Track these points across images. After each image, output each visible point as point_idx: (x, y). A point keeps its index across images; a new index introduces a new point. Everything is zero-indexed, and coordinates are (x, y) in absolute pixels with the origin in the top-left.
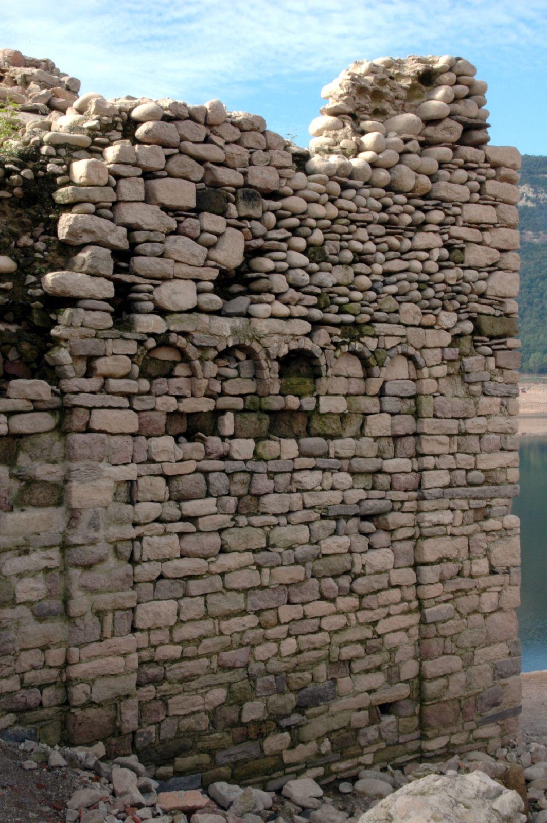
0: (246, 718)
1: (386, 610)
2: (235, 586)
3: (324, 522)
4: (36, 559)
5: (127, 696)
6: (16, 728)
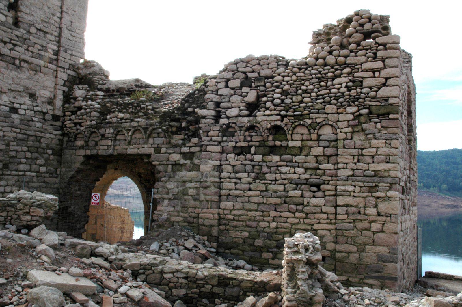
0: (256, 244)
1: (318, 221)
2: (253, 201)
3: (290, 185)
5: (214, 226)
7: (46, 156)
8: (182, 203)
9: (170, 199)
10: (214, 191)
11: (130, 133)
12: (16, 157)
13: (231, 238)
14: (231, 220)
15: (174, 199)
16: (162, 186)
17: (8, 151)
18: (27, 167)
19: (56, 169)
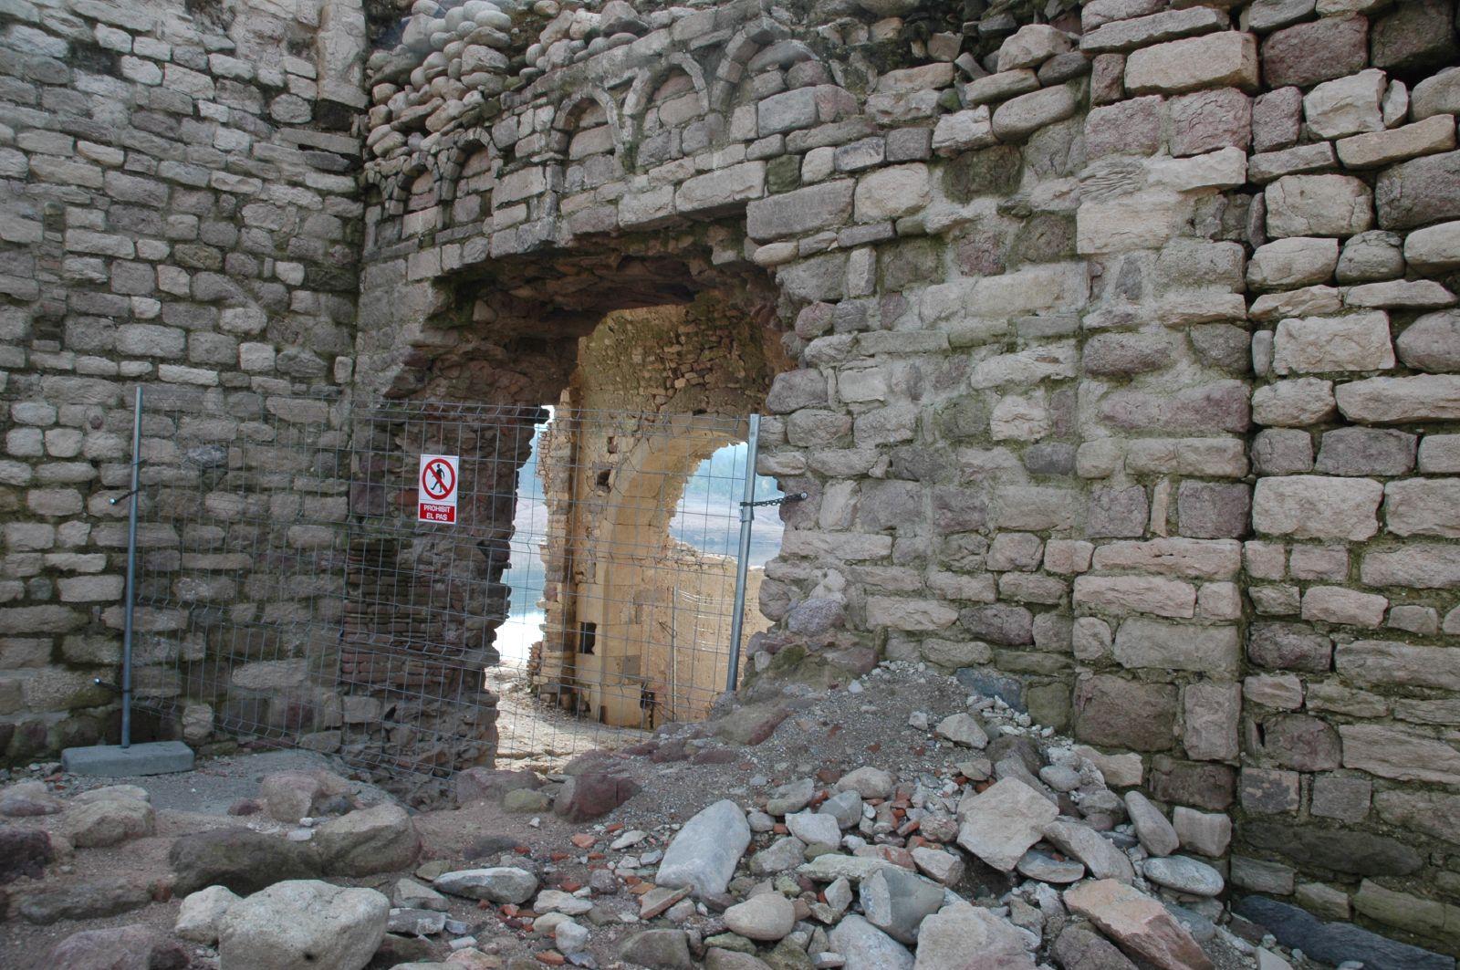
4: (1027, 363)
5: (1201, 676)
6: (985, 671)
7: (272, 291)
8: (943, 505)
9: (863, 477)
10: (1198, 393)
11: (631, 99)
12: (105, 286)
13: (1365, 785)
14: (1363, 633)
15: (888, 476)
16: (814, 395)
17: (57, 253)
18: (168, 341)
19: (331, 358)
